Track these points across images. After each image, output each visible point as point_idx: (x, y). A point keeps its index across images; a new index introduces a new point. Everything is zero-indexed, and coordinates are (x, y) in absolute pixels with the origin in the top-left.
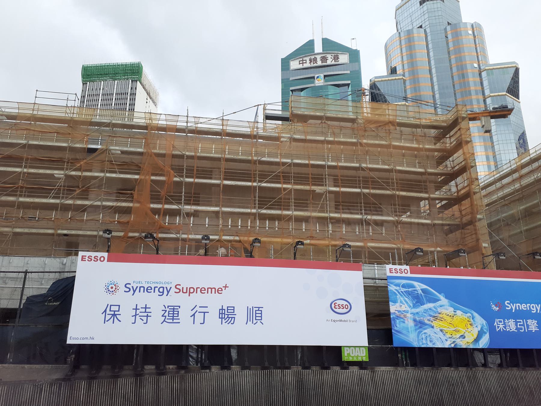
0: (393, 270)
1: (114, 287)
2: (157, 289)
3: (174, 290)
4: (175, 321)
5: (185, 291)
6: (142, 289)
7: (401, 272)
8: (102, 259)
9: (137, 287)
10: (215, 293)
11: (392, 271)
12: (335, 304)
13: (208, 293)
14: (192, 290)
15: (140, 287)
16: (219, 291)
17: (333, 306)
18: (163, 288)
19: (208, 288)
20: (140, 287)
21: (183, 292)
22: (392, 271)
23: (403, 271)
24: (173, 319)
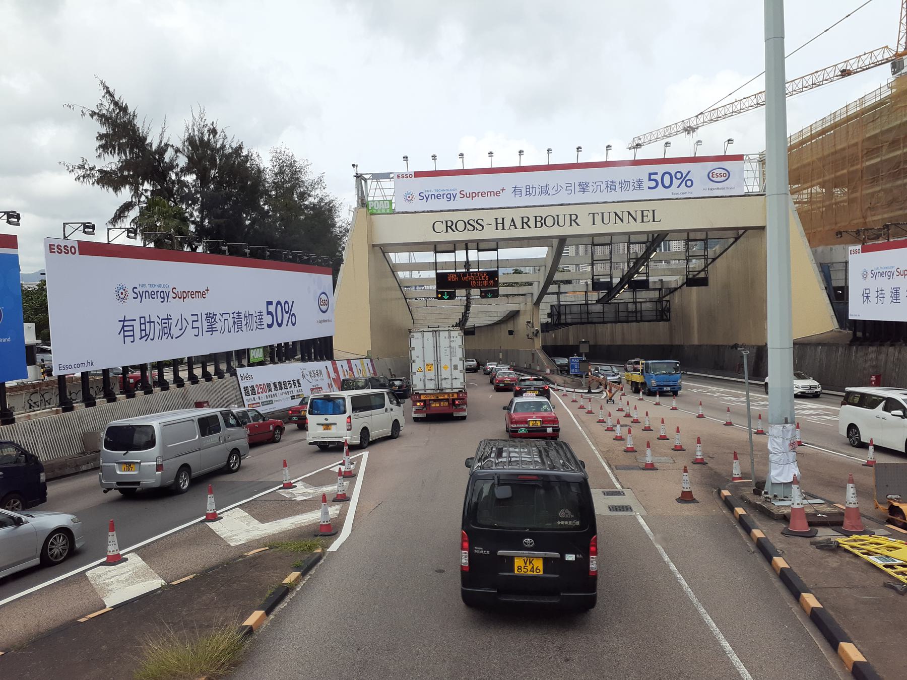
0: (55, 247)
1: (410, 195)
2: (445, 196)
3: (459, 195)
4: (641, 189)
5: (468, 196)
6: (433, 196)
7: (66, 252)
8: (411, 176)
9: (429, 195)
10: (494, 196)
11: (54, 249)
12: (712, 173)
13: (488, 196)
14: (474, 195)
15: (431, 195)
16: (497, 194)
17: (711, 175)
18: (450, 194)
19: (488, 192)
20: (431, 195)
21: (467, 197)
22: (54, 249)
23: (69, 249)
24: (640, 188)
